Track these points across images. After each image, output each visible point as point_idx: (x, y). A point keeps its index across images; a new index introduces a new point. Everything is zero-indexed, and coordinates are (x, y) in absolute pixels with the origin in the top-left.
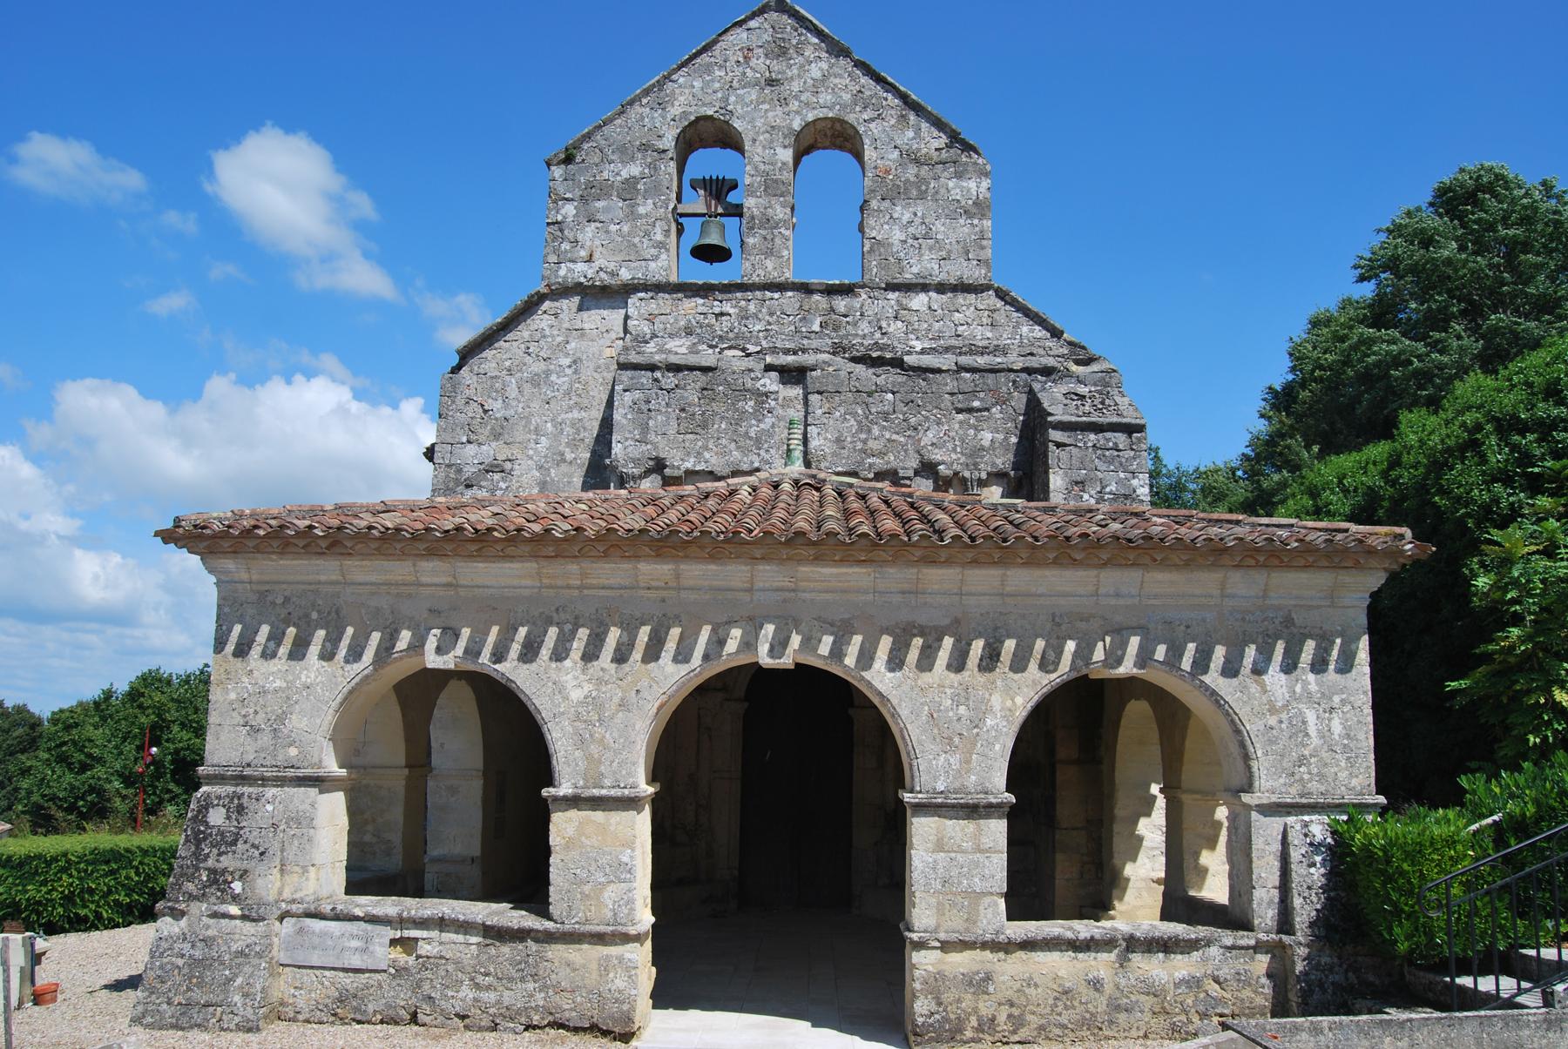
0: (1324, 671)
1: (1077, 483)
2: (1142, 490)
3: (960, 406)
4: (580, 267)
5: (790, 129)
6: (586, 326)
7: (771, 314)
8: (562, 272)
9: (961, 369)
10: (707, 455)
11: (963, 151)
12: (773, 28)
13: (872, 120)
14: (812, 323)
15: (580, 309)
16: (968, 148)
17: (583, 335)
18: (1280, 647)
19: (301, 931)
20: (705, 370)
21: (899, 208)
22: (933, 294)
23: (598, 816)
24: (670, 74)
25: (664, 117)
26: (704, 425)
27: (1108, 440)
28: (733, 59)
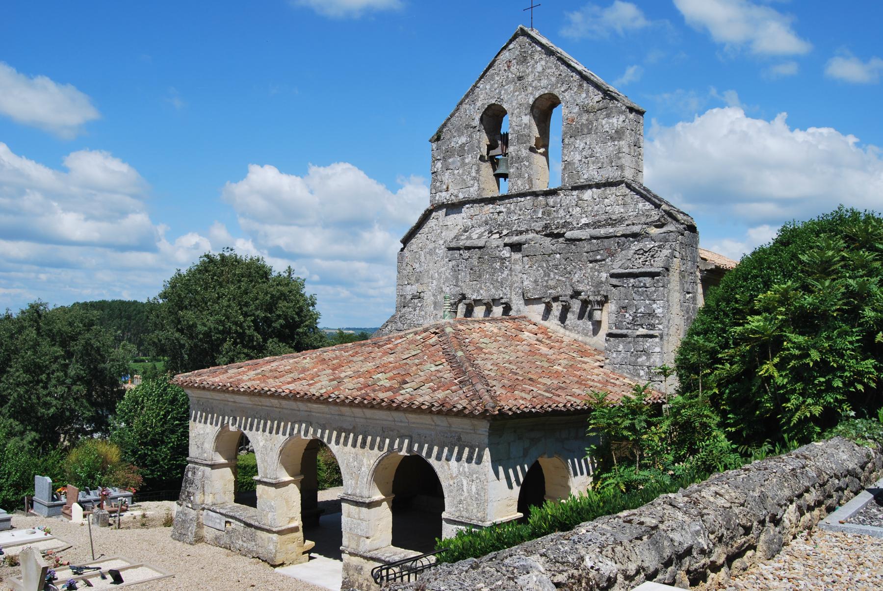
0: (471, 462)
1: (623, 308)
2: (659, 310)
3: (591, 259)
4: (444, 194)
5: (528, 104)
6: (449, 223)
7: (520, 210)
8: (437, 198)
9: (593, 238)
10: (481, 292)
11: (610, 100)
12: (520, 46)
13: (566, 90)
14: (538, 213)
15: (446, 215)
16: (613, 98)
17: (447, 228)
18: (456, 449)
19: (207, 514)
20: (480, 248)
21: (578, 141)
22: (594, 190)
23: (266, 487)
24: (476, 84)
25: (474, 108)
26: (480, 277)
27: (640, 282)
28: (503, 69)
